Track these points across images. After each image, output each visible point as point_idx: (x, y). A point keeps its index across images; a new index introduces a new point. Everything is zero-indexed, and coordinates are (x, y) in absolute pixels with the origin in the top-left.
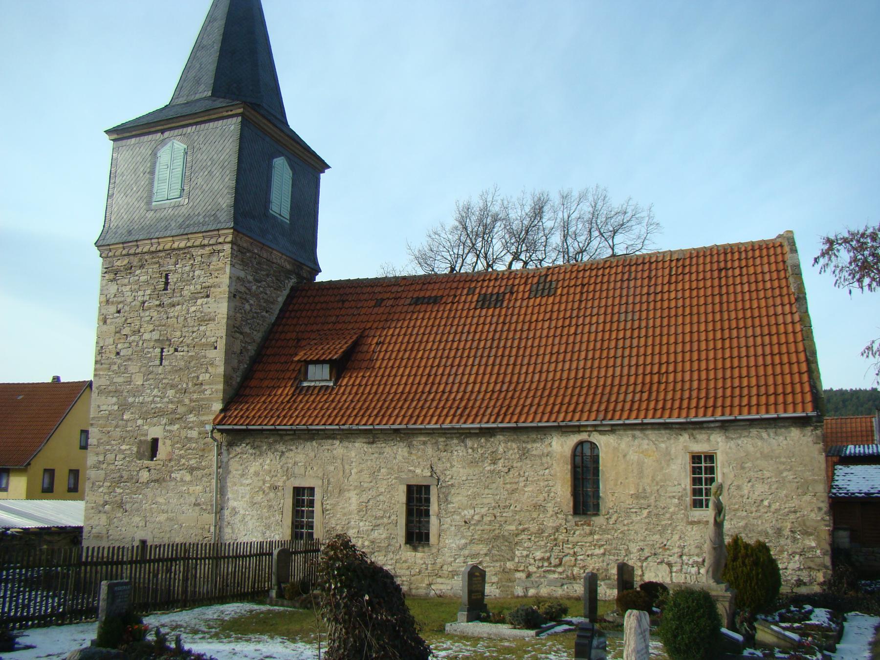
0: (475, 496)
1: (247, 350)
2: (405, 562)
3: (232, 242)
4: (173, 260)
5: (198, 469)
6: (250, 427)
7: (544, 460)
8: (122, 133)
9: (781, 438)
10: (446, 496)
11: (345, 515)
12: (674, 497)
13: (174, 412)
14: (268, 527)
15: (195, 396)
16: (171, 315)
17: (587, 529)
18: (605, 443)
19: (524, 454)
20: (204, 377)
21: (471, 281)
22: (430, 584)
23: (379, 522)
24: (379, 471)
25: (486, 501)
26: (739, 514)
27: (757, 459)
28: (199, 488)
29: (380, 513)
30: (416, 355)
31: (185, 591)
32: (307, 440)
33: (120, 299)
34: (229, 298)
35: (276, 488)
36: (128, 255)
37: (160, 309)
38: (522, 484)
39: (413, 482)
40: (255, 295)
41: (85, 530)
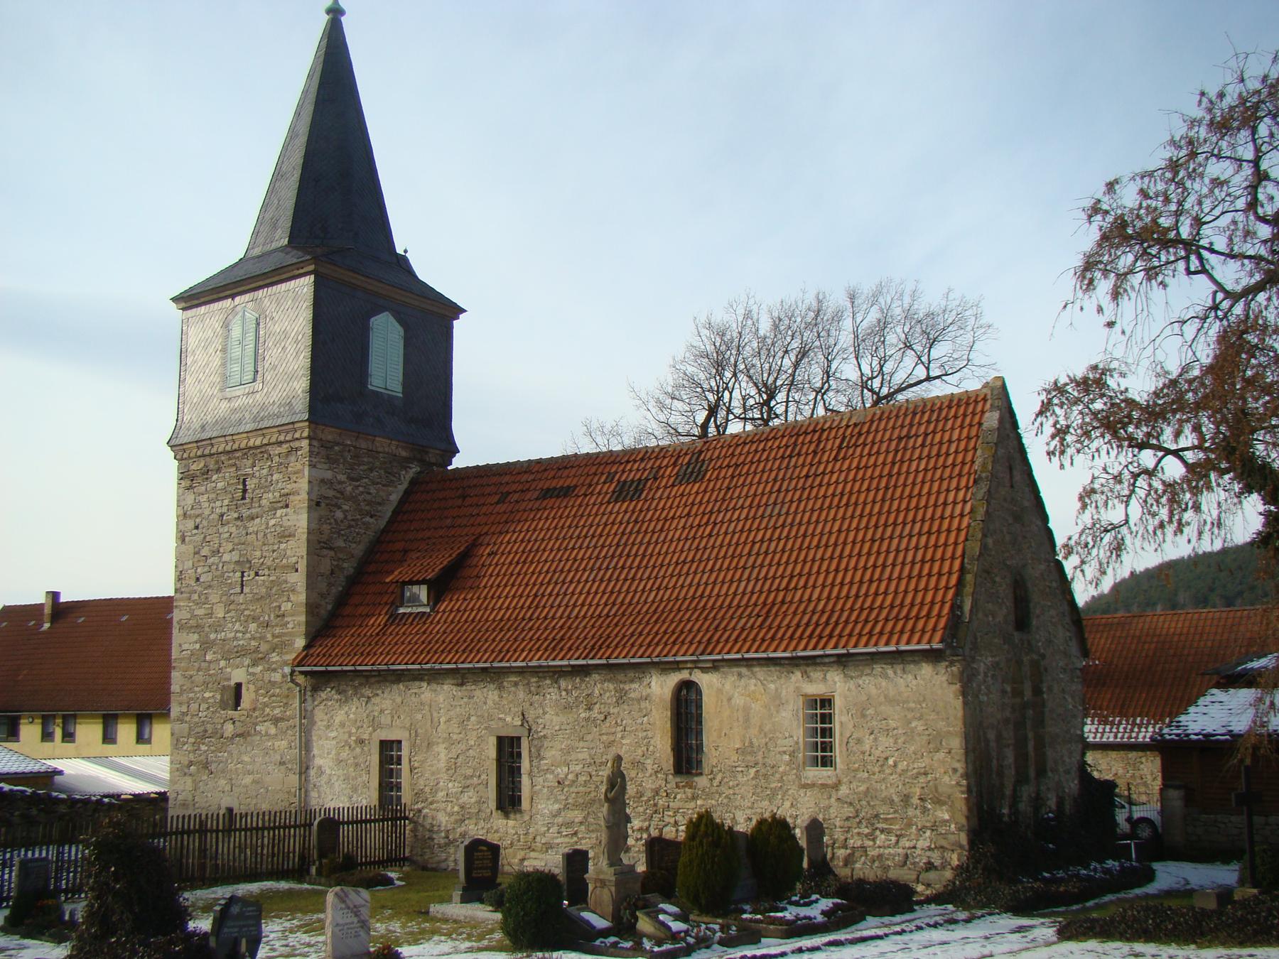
0: (569, 751)
2: (497, 831)
3: (309, 437)
4: (250, 462)
5: (282, 719)
6: (330, 668)
7: (643, 705)
9: (910, 677)
10: (539, 751)
11: (433, 774)
12: (785, 752)
13: (256, 650)
14: (355, 789)
15: (277, 630)
16: (250, 530)
17: (689, 791)
18: (705, 680)
19: (621, 698)
20: (287, 607)
21: (614, 463)
22: (523, 860)
23: (469, 782)
24: (469, 719)
25: (581, 756)
27: (881, 704)
28: (284, 743)
29: (469, 772)
32: (393, 682)
34: (309, 507)
36: (203, 456)
37: (239, 523)
40: (351, 498)
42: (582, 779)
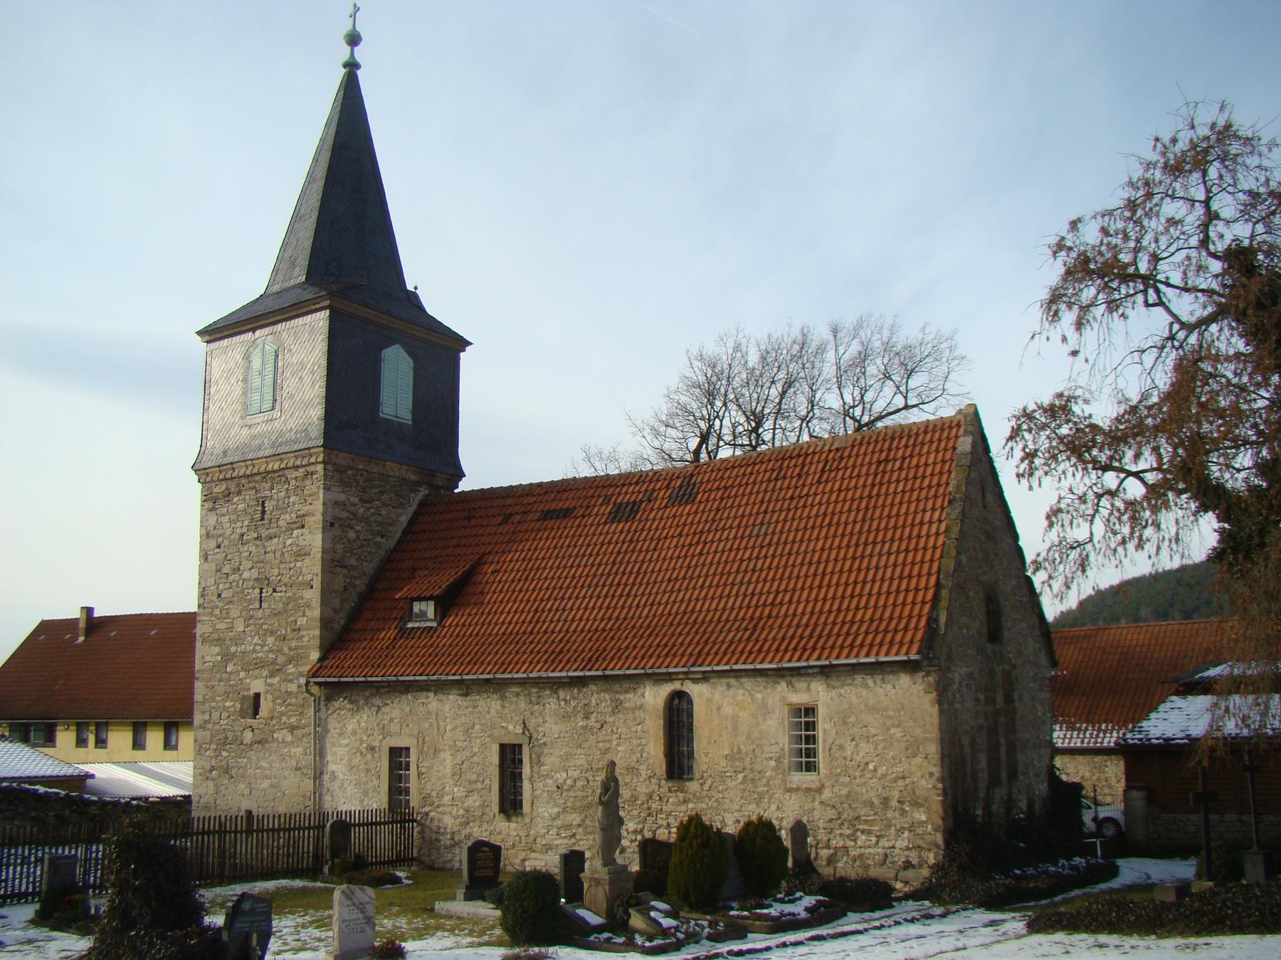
0: (568, 756)
1: (354, 586)
2: (499, 833)
3: (324, 462)
5: (298, 727)
7: (637, 713)
8: (214, 333)
9: (889, 686)
10: (539, 757)
13: (274, 662)
14: (366, 794)
15: (294, 644)
17: (681, 795)
18: (697, 691)
19: (617, 707)
20: (302, 621)
22: (524, 860)
23: (473, 786)
24: (473, 727)
25: (579, 762)
26: (842, 779)
27: (861, 712)
28: (300, 750)
29: (474, 777)
30: (870, 527)
31: (222, 865)
33: (220, 532)
34: (323, 527)
35: (373, 749)
36: (225, 479)
37: (258, 542)
38: (615, 743)
39: (506, 741)
41: (194, 799)
42: (580, 784)
